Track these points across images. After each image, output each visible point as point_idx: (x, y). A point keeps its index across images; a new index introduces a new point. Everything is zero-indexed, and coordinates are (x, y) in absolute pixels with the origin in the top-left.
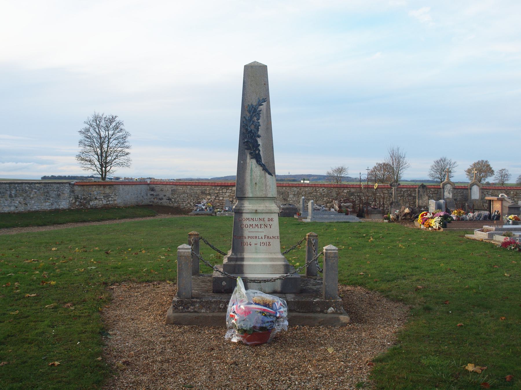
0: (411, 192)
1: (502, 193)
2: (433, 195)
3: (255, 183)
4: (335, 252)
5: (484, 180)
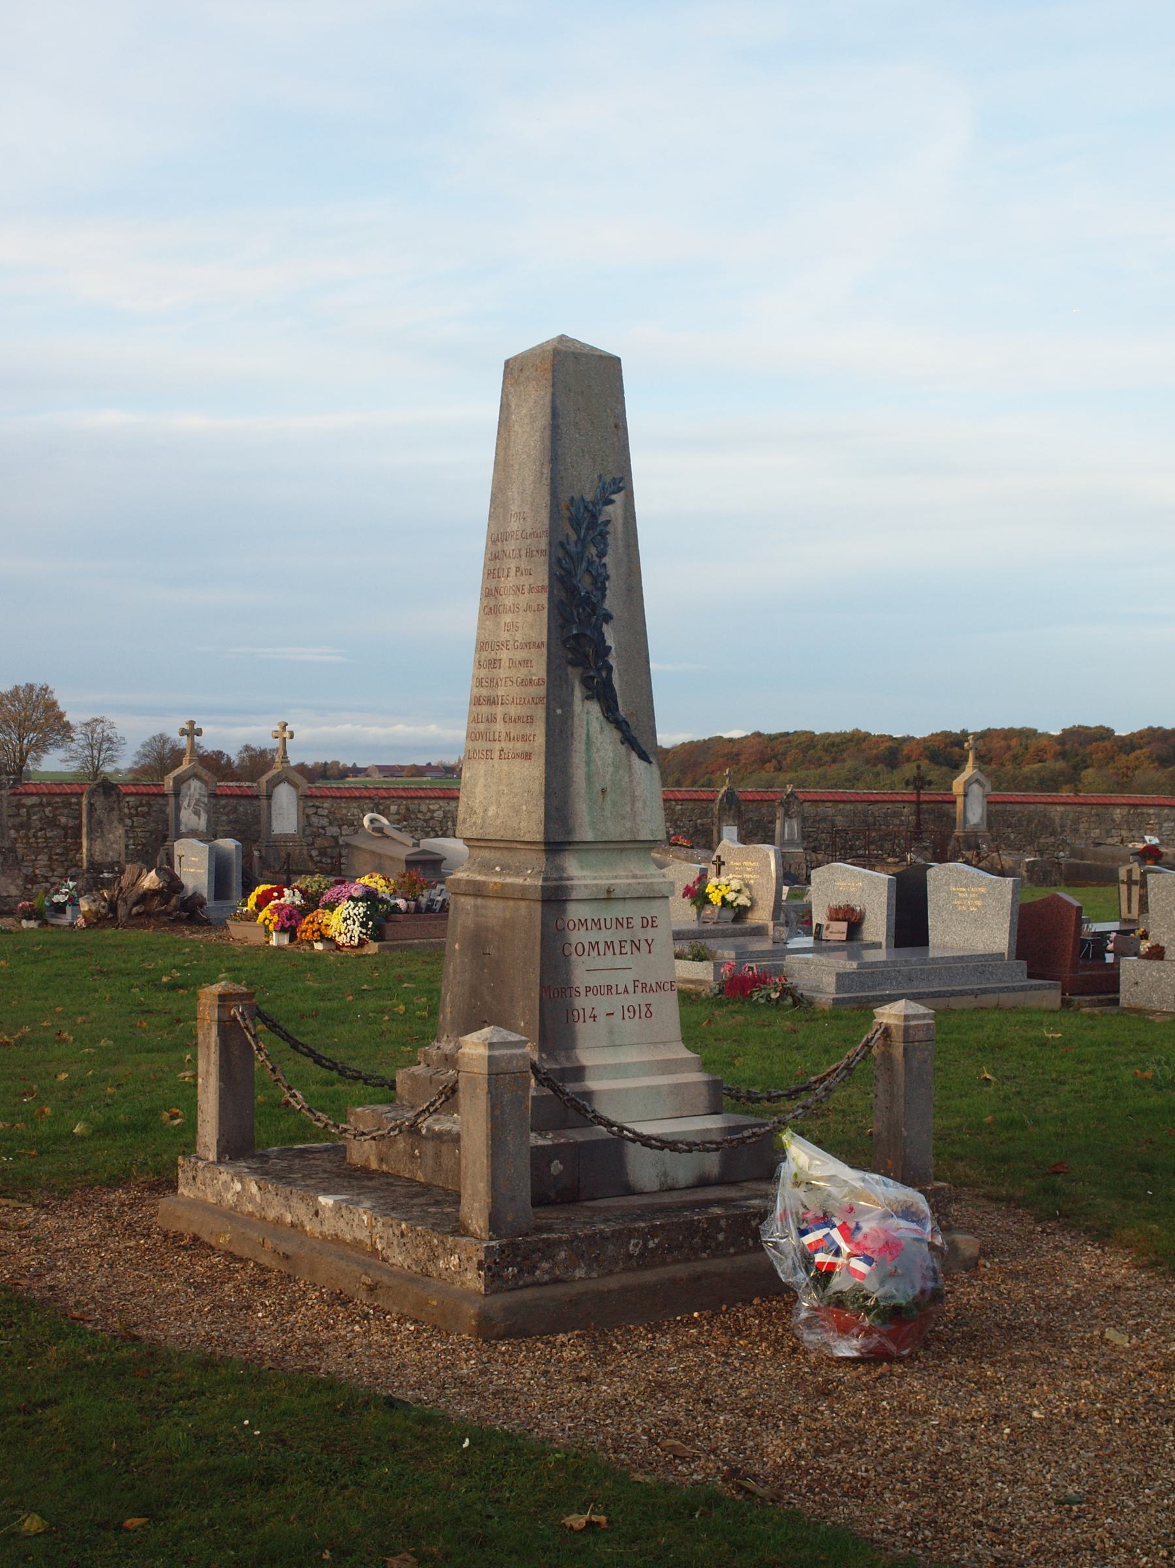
0: (56, 809)
1: (373, 812)
2: (135, 819)
3: (600, 788)
4: (928, 1024)
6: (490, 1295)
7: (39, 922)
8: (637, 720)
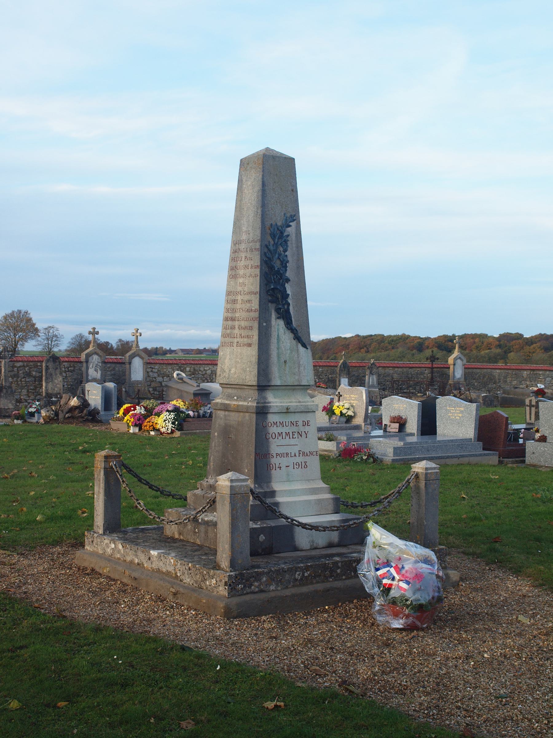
0: (31, 368)
2: (67, 373)
4: (436, 472)
5: (23, 345)
6: (230, 598)
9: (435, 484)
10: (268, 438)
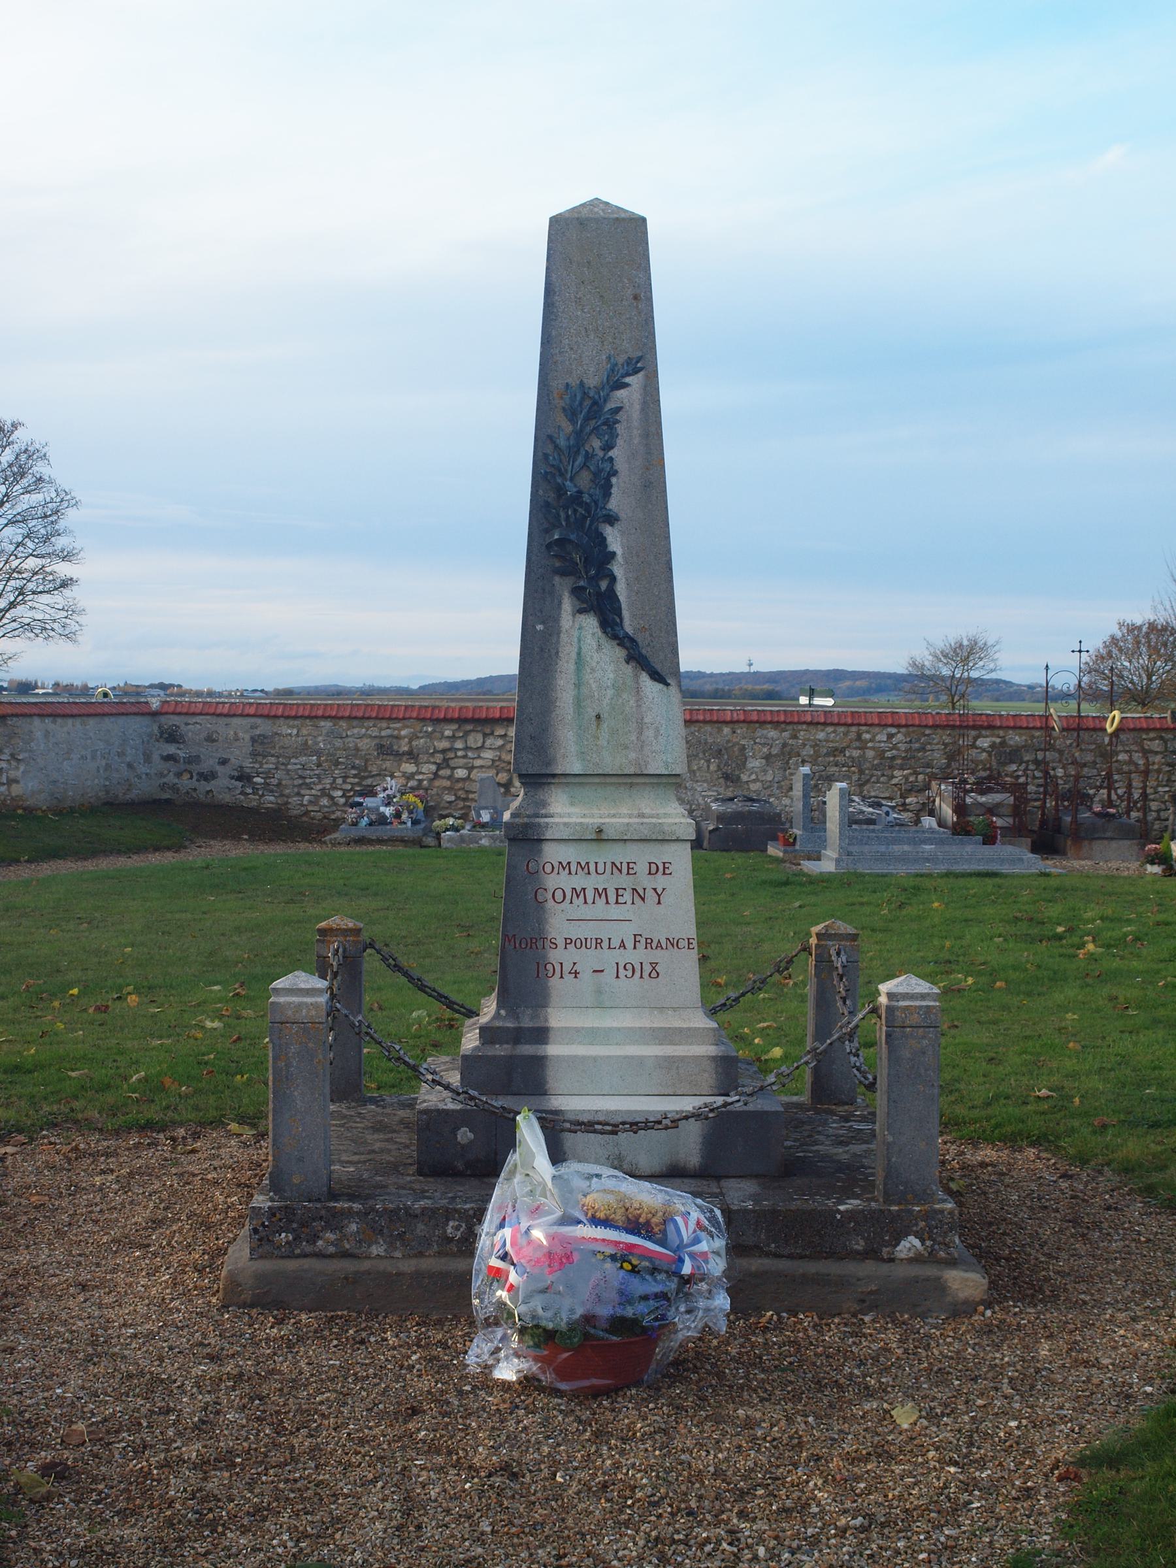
3: (594, 714)
4: (928, 1007)
6: (256, 1259)
7: (1164, 867)
8: (651, 635)
9: (924, 1037)
10: (540, 899)
